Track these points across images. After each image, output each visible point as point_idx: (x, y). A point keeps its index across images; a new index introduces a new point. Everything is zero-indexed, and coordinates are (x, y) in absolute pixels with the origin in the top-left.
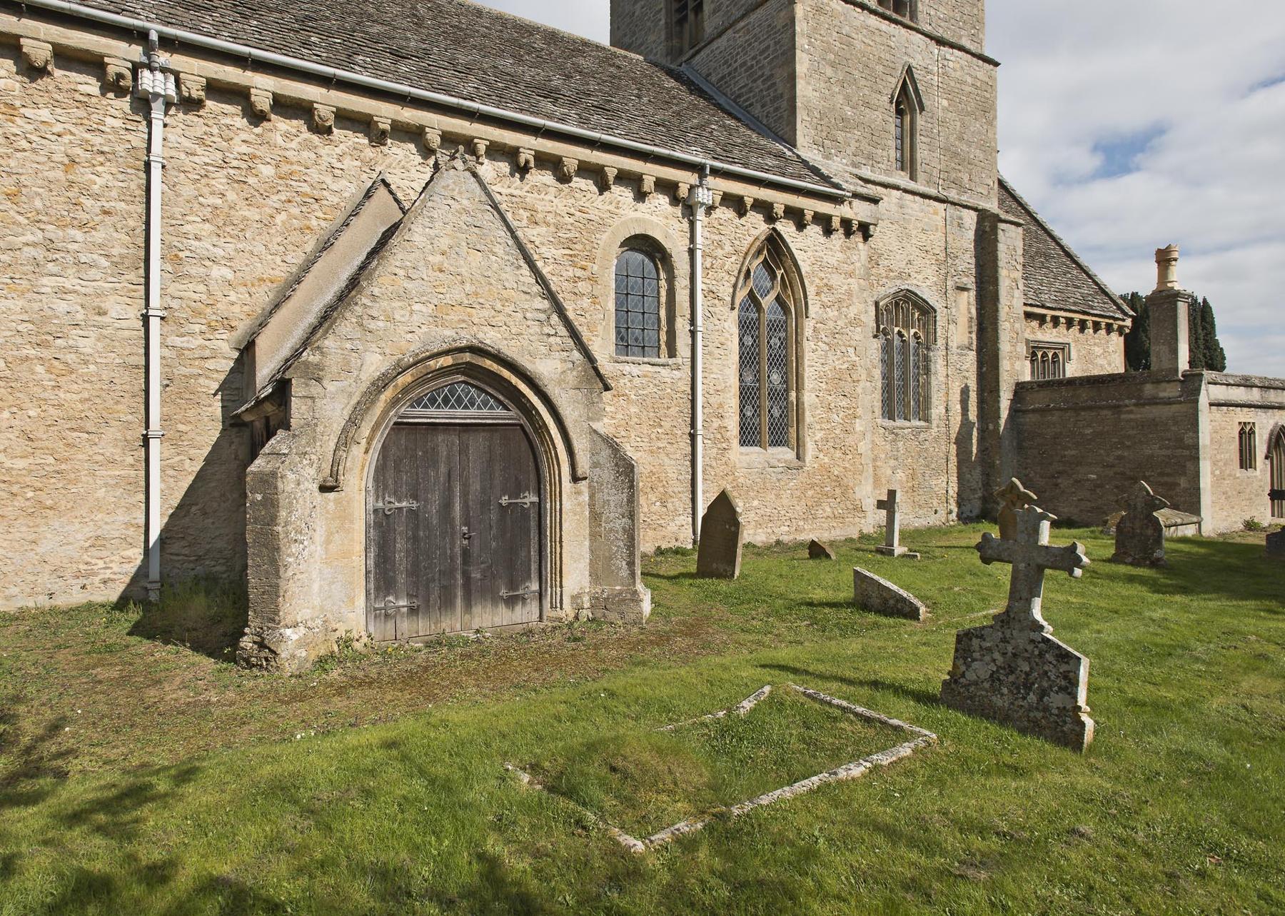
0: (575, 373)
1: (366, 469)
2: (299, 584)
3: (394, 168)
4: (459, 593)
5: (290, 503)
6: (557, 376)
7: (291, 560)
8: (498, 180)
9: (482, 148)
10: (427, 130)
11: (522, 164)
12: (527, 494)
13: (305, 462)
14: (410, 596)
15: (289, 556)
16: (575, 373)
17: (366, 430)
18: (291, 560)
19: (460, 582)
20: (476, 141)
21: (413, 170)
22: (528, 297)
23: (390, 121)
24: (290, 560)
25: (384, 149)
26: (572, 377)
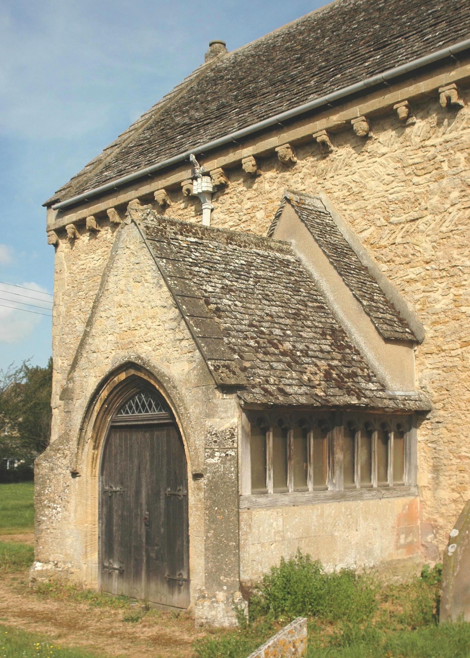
0: (195, 372)
1: (98, 461)
2: (51, 535)
3: (340, 169)
4: (144, 568)
5: (44, 482)
6: (184, 377)
7: (44, 518)
8: (431, 132)
9: (402, 111)
10: (277, 149)
11: (161, 203)
12: (181, 487)
13: (58, 455)
14: (121, 562)
15: (42, 515)
16: (195, 372)
17: (90, 433)
18: (44, 518)
19: (145, 559)
20: (395, 107)
21: (355, 163)
22: (165, 310)
23: (324, 132)
24: (43, 518)
25: (332, 156)
26: (193, 378)
